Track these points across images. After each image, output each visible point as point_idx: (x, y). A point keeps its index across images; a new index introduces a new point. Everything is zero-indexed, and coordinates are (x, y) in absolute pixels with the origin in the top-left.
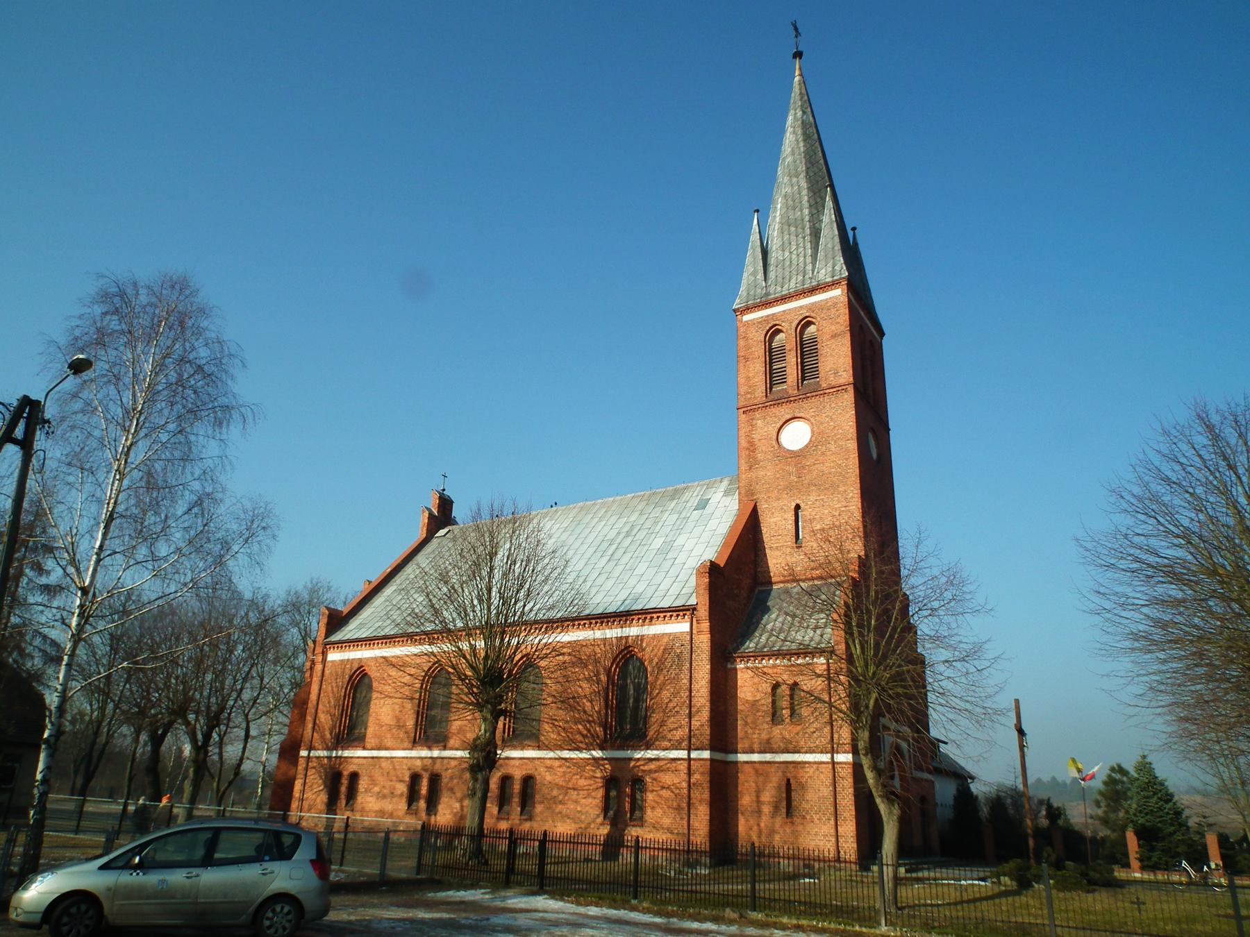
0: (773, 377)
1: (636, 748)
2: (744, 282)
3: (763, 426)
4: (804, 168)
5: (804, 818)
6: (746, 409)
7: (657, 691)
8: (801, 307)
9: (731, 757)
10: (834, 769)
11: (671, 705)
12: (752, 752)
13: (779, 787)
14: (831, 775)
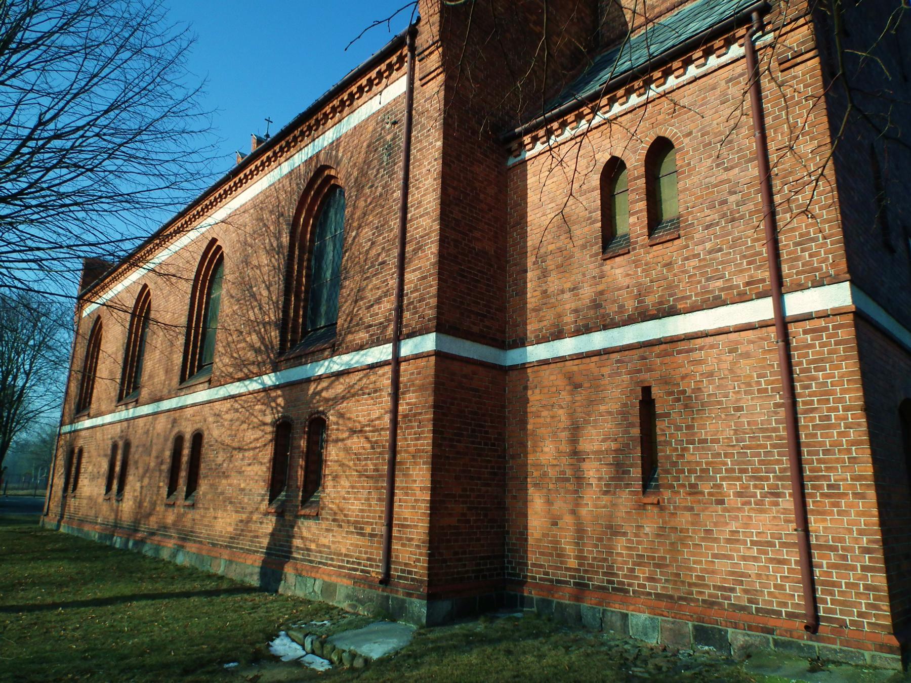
1: (316, 356)
5: (694, 490)
7: (354, 234)
9: (513, 357)
10: (785, 337)
11: (373, 252)
13: (623, 414)
14: (775, 361)
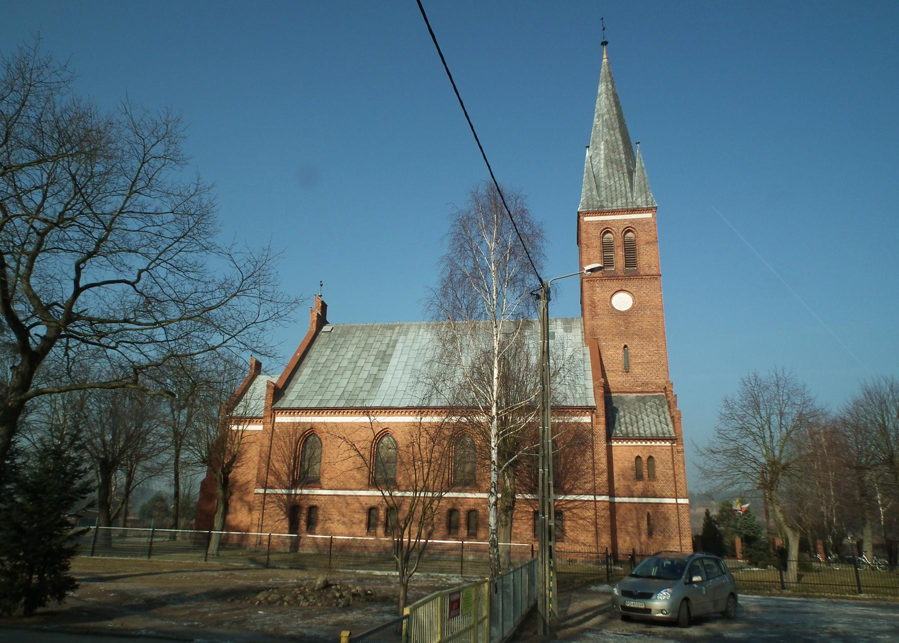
0: (608, 262)
2: (583, 194)
3: (600, 292)
4: (618, 126)
6: (588, 279)
8: (625, 220)
12: (633, 496)
